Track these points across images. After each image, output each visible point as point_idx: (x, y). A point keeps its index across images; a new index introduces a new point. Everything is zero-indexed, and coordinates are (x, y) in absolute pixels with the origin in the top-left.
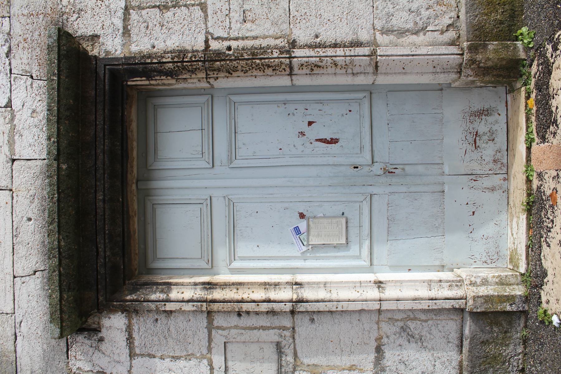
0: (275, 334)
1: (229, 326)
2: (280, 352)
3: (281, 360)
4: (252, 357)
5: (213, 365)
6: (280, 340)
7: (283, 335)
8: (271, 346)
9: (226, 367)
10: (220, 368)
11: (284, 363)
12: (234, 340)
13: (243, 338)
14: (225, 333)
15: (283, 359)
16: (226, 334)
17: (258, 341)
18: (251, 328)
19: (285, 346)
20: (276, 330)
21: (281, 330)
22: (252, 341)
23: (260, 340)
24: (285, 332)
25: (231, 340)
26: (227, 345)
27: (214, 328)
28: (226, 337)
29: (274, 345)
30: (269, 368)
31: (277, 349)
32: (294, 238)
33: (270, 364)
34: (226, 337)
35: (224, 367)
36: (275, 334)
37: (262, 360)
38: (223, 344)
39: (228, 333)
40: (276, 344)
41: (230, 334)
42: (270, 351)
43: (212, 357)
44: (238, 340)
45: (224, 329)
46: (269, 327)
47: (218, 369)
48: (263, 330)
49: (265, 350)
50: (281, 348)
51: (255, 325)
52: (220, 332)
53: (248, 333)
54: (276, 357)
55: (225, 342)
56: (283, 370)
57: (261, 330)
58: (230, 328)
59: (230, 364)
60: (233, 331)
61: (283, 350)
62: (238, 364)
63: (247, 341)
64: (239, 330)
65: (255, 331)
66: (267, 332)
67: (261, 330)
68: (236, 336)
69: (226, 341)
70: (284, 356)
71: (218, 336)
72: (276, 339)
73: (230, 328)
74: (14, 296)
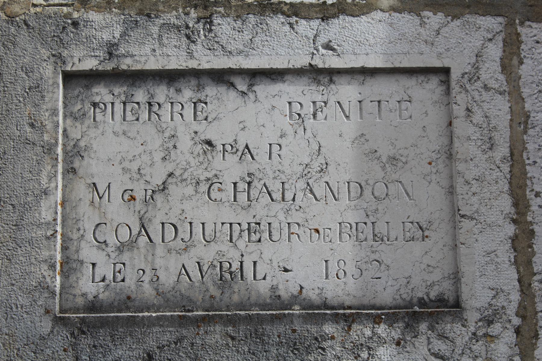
0: (497, 292)
1: (526, 91)
2: (416, 317)
3: (377, 320)
4: (380, 190)
5: (343, 20)
6: (472, 317)
7: (496, 329)
8: (436, 276)
9: (331, 74)
10: (328, 47)
11: (362, 331)
12: (459, 110)
13: (468, 147)
14: (491, 71)
15: (382, 329)
16: (484, 76)
17: (456, 215)
18: (523, 187)
19: (442, 337)
20: (515, 297)
21: (517, 321)
22: (461, 188)
23: (466, 224)
24: (510, 336)
25: (461, 99)
26: (434, 82)
27: (510, 24)
28: (473, 76)
29: (445, 288)
30: (333, 268)
31: (422, 303)
32: (360, 133)
33: (351, 269)
34: (473, 76)
35: (335, 62)
36: (497, 292)
37: (370, 234)
38: (437, 64)
39: (493, 84)
40: (450, 296)
41: (486, 96)
42: (412, 270)
43: (377, 15)
44: (461, 127)
45: (506, 67)
46: (529, 263)
47: (322, 39)
48: (514, 239)
49: (418, 248)
50: (434, 318)
51: (535, 203)
52: (495, 51)
53: (496, 174)
54: (386, 294)
55: (446, 71)
56: (329, 329)
57: (511, 229)
58: (515, 94)
59: (348, 92)
60: (500, 109)
61: (423, 327)
62: (350, 128)
63: (461, 167)
64: (507, 134)
65: (506, 203)
66: (505, 255)
67: (511, 229)
68: (478, 118)
69: (455, 75)
70: (396, 334)
71: (475, 41)
72: (476, 296)
73: (515, 94)
74: (191, 232)
